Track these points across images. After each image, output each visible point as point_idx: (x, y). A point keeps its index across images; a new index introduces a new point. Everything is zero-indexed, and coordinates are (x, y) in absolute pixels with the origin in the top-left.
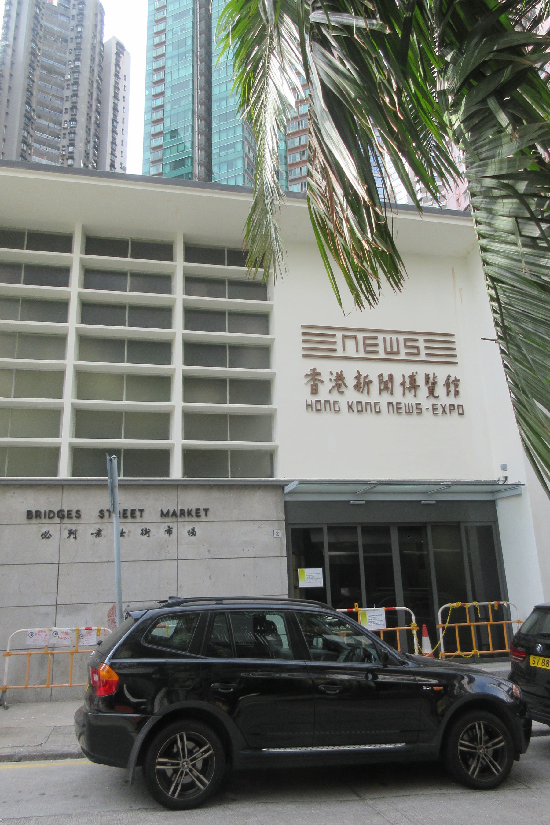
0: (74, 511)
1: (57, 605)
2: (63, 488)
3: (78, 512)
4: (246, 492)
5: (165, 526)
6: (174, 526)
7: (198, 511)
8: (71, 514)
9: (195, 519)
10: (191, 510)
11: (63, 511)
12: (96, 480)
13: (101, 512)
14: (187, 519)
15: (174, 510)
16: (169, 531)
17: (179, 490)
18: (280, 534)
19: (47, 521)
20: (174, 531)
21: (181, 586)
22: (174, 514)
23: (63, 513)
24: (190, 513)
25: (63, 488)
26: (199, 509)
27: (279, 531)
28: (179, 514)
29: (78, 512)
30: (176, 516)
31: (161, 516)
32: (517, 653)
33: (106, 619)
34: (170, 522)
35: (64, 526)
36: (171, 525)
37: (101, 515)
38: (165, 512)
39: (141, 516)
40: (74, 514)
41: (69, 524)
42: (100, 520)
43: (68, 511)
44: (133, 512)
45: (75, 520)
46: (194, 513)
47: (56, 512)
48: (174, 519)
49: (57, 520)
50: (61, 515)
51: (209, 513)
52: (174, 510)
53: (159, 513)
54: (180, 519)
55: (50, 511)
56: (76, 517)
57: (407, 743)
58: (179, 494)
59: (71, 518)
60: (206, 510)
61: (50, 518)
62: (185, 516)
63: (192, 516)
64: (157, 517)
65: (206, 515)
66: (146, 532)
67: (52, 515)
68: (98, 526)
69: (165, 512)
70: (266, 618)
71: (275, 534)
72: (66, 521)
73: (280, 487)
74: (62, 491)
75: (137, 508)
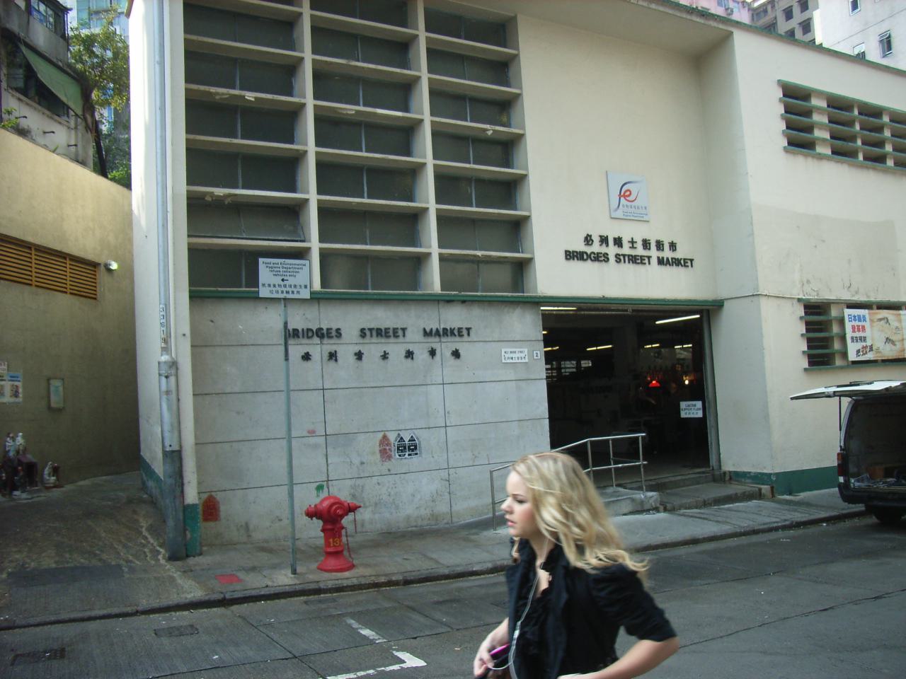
0: (334, 329)
1: (326, 435)
2: (438, 303)
3: (338, 330)
4: (506, 310)
5: (427, 347)
6: (388, 348)
7: (460, 330)
8: (331, 333)
9: (457, 339)
10: (454, 329)
11: (322, 329)
12: (469, 296)
13: (362, 330)
14: (449, 339)
15: (437, 329)
16: (433, 353)
17: (321, 305)
18: (539, 355)
19: (305, 341)
20: (438, 352)
21: (448, 413)
22: (437, 333)
23: (322, 332)
24: (452, 331)
25: (438, 303)
26: (462, 328)
27: (539, 352)
28: (441, 333)
29: (338, 330)
30: (439, 336)
31: (424, 336)
32: (365, 589)
33: (377, 449)
34: (434, 342)
35: (325, 347)
36: (434, 346)
37: (338, 335)
38: (428, 330)
39: (404, 336)
40: (334, 333)
41: (329, 346)
42: (361, 341)
43: (328, 329)
44: (395, 330)
45: (334, 341)
46: (456, 332)
47: (315, 331)
48: (437, 339)
49: (316, 340)
50: (321, 334)
51: (472, 333)
52: (437, 329)
53: (422, 333)
54: (444, 339)
55: (309, 330)
56: (336, 336)
57: (545, 591)
58: (321, 309)
59: (332, 337)
60: (468, 329)
61: (308, 337)
62: (447, 336)
63: (455, 336)
64: (419, 336)
65: (469, 334)
66: (409, 354)
67: (310, 334)
68: (357, 349)
69: (428, 330)
70: (680, 414)
71: (535, 355)
72: (326, 341)
73: (536, 302)
74: (319, 307)
75: (399, 326)
